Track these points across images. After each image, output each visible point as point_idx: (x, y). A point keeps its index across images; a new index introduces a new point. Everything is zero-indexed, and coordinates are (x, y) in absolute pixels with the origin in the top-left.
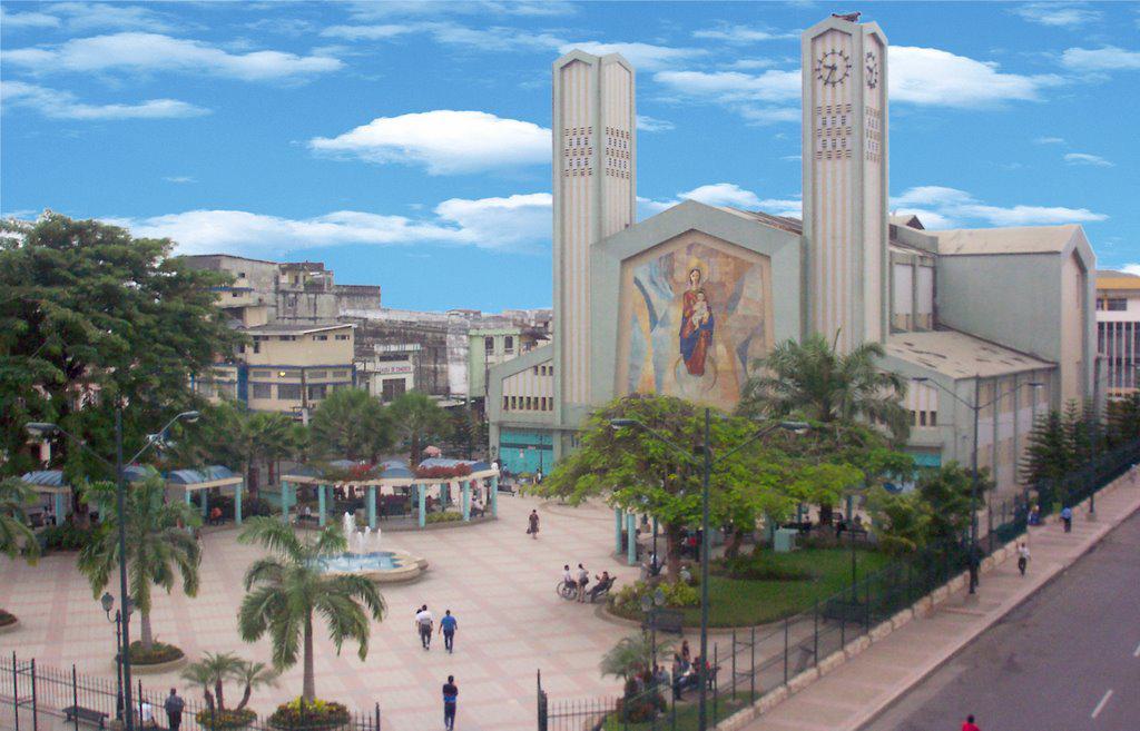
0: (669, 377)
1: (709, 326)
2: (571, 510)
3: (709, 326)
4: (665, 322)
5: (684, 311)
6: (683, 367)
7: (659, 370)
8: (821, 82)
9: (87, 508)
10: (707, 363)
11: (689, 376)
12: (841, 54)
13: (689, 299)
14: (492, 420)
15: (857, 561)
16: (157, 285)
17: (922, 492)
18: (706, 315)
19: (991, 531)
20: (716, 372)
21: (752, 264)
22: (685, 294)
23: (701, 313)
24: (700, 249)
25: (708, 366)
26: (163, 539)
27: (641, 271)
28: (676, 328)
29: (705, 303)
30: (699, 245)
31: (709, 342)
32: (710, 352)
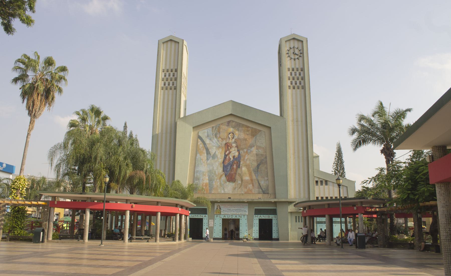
0: (216, 183)
1: (237, 160)
2: (45, 58)
3: (237, 160)
4: (214, 156)
5: (226, 152)
6: (224, 178)
7: (211, 180)
8: (300, 48)
9: (237, 231)
10: (237, 176)
11: (228, 183)
12: (297, 48)
13: (228, 146)
14: (76, 119)
15: (81, 188)
16: (67, 159)
17: (240, 238)
18: (237, 154)
19: (261, 249)
20: (242, 180)
21: (260, 131)
22: (225, 144)
23: (234, 152)
24: (234, 124)
25: (237, 177)
26: (350, 227)
27: (203, 133)
28: (221, 160)
29: (236, 148)
30: (233, 121)
31: (238, 166)
32: (239, 171)
